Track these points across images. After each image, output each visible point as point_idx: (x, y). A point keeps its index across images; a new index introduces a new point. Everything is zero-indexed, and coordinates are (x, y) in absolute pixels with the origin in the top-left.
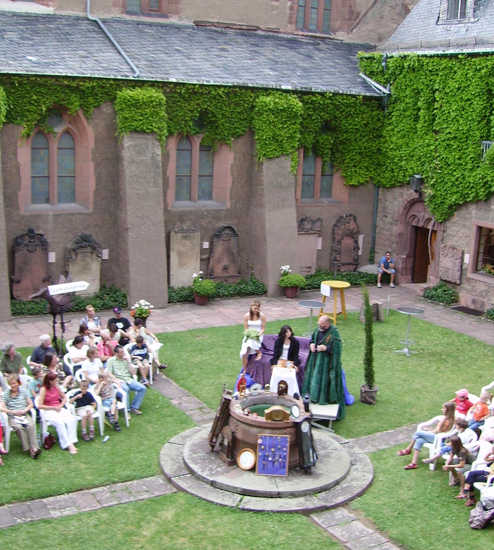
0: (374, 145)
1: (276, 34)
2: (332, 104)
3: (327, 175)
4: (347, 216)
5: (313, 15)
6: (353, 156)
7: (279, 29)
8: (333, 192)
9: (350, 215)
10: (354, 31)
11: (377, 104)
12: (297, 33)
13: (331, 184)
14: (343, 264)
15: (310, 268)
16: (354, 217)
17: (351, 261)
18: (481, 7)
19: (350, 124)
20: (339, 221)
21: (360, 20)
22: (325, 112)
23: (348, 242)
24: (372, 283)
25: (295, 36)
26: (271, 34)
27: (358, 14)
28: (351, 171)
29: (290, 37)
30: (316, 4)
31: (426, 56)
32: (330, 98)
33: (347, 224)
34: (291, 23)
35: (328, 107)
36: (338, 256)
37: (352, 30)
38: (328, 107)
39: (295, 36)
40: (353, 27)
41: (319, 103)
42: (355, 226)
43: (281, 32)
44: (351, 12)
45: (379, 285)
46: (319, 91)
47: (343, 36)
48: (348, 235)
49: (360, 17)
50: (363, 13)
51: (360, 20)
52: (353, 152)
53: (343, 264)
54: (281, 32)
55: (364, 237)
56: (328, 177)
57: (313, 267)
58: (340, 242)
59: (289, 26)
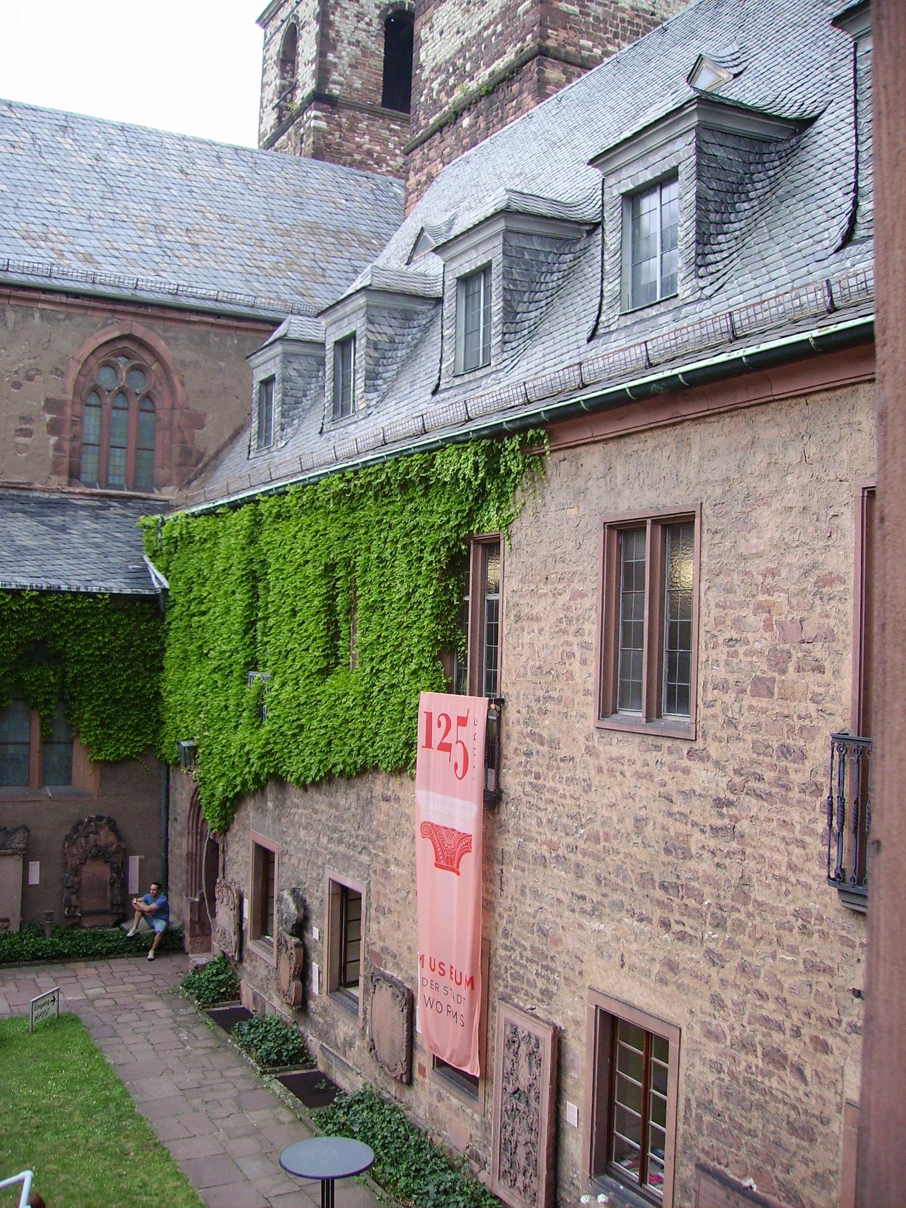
0: (148, 686)
1: (24, 493)
2: (39, 610)
3: (59, 743)
4: (90, 820)
5: (117, 459)
6: (99, 706)
7: (31, 484)
8: (74, 775)
9: (99, 818)
10: (194, 483)
11: (150, 608)
12: (71, 490)
13: (70, 760)
14: (90, 914)
15: (7, 920)
16: (110, 821)
17: (108, 906)
18: (296, 421)
19: (86, 647)
20: (75, 829)
21: (205, 466)
22: (27, 625)
23: (98, 871)
24: (130, 951)
25: (65, 496)
26: (15, 492)
27: (201, 455)
28: (96, 735)
29: (55, 496)
30: (124, 441)
31: (195, 516)
32: (33, 599)
33: (92, 836)
34: (57, 473)
35: (33, 616)
36: (74, 897)
37: (189, 483)
38: (33, 616)
39: (65, 496)
40: (191, 476)
41: (10, 609)
42: (112, 838)
43: (36, 490)
44: (186, 452)
45: (151, 954)
46: (14, 587)
47: (172, 493)
48: (95, 858)
49: (206, 459)
50: (211, 452)
51: (205, 466)
52: (98, 699)
53: (90, 914)
54: (36, 490)
55: (140, 860)
56: (62, 746)
57: (12, 919)
58: (76, 871)
59: (54, 478)
